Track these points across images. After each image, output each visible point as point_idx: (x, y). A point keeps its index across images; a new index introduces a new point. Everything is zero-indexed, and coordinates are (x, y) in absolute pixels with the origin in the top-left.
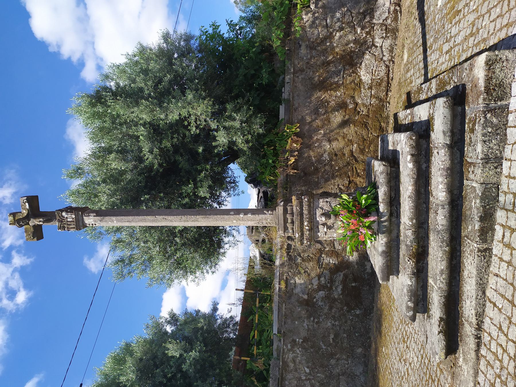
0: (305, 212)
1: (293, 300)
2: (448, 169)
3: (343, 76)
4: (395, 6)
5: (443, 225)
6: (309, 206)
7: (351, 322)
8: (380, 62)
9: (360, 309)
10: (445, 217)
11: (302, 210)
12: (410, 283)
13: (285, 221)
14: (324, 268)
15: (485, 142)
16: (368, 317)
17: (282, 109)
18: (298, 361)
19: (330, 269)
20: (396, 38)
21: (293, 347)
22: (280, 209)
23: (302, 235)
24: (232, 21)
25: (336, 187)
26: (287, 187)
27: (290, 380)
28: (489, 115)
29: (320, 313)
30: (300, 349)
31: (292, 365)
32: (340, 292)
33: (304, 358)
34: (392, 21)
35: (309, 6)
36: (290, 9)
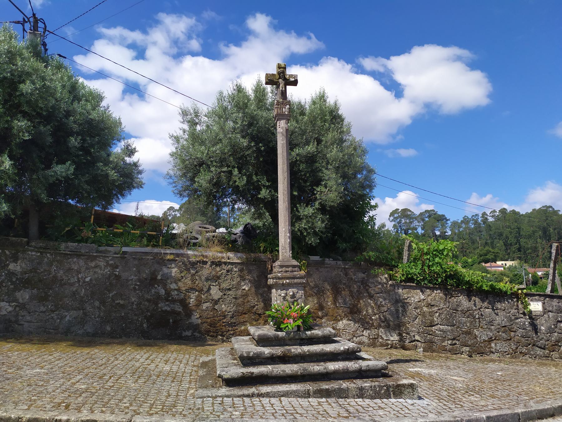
0: (296, 281)
1: (156, 266)
2: (348, 370)
3: (342, 307)
4: (391, 345)
5: (314, 369)
6: (300, 283)
7: (136, 320)
8: (352, 335)
9: (148, 327)
10: (319, 370)
11: (297, 279)
12: (266, 353)
13: (287, 266)
14: (186, 294)
15: (371, 387)
16: (140, 335)
17: (317, 258)
18: (97, 270)
19: (186, 300)
20: (369, 346)
21: (111, 265)
22: (295, 263)
23: (279, 278)
24: (375, 219)
25: (256, 303)
26: (256, 261)
27: (78, 263)
28: (385, 388)
29: (144, 291)
30: (109, 272)
31: (93, 264)
32: (164, 309)
33: (100, 277)
34: (380, 342)
35: (391, 280)
36: (389, 265)
